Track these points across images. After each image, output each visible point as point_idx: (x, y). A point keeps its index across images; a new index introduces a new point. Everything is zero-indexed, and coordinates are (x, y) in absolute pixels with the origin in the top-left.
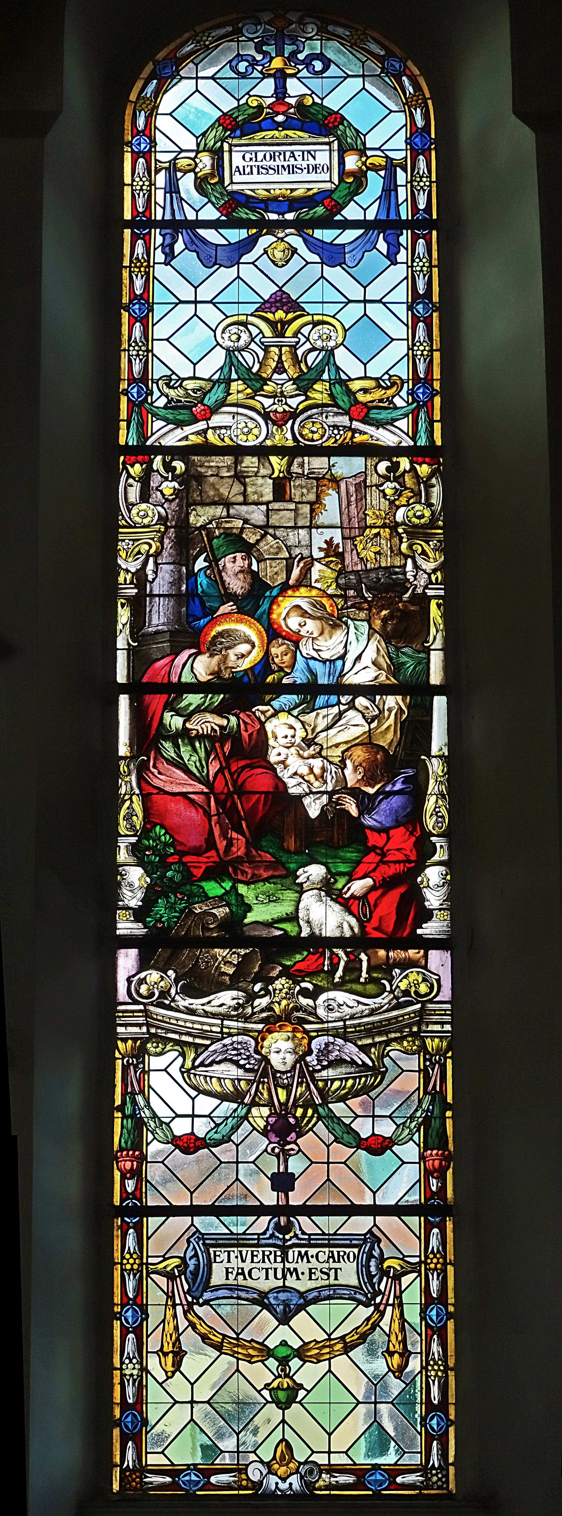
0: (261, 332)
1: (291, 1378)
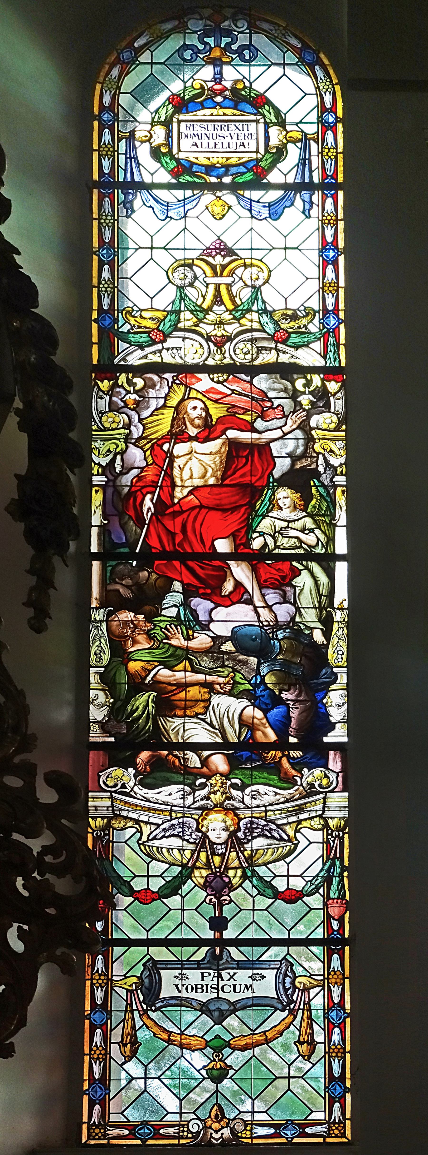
0: (204, 273)
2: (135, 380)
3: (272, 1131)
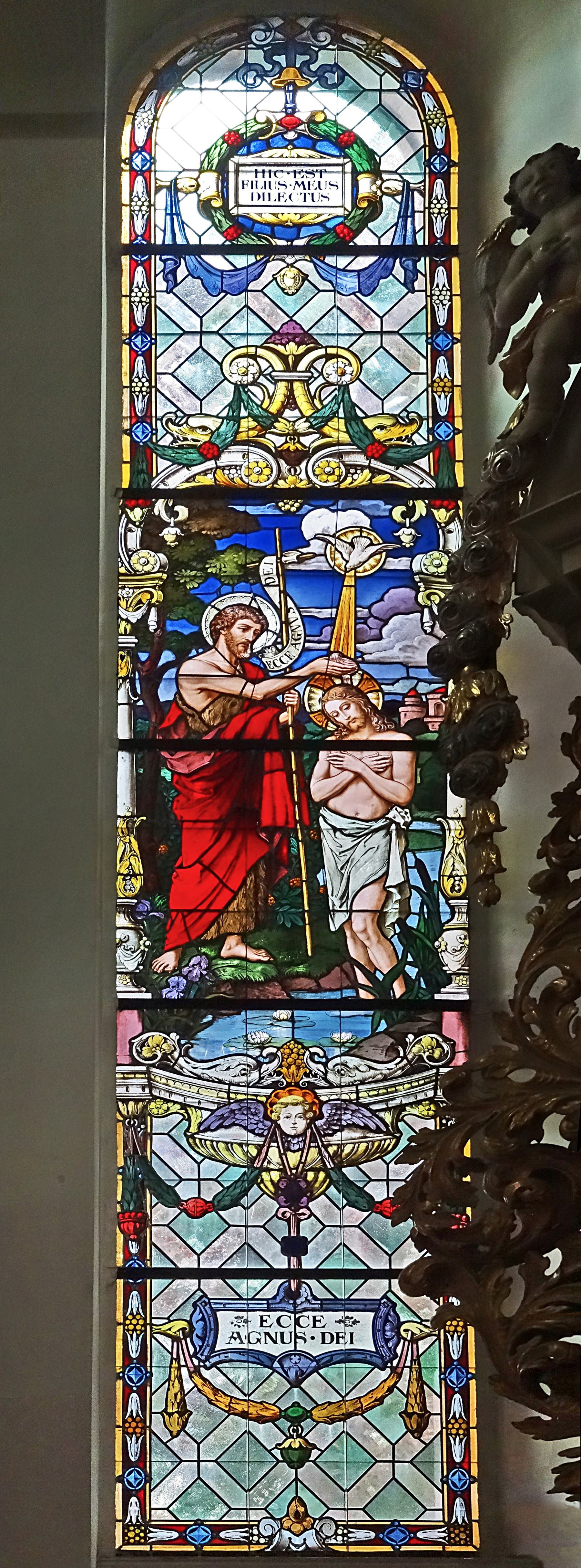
0: (271, 366)
1: (304, 1438)
2: (177, 508)
3: (372, 1535)
